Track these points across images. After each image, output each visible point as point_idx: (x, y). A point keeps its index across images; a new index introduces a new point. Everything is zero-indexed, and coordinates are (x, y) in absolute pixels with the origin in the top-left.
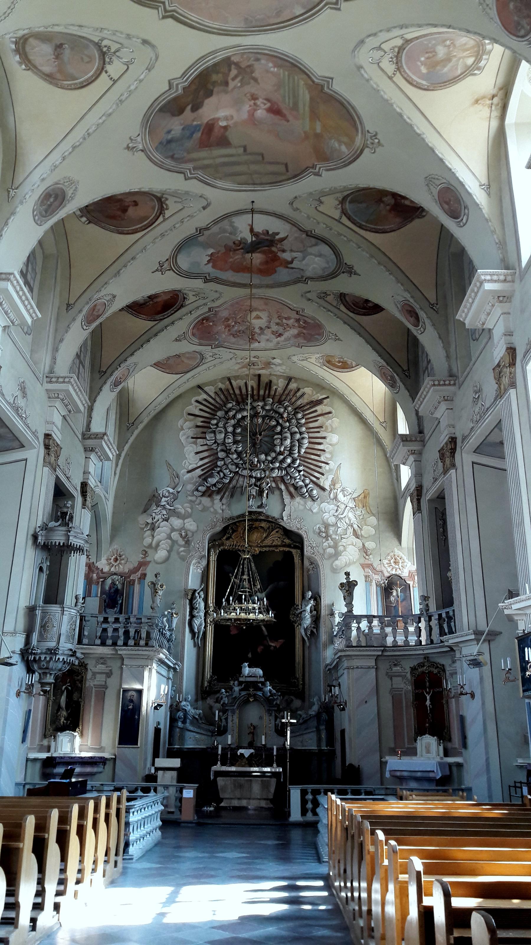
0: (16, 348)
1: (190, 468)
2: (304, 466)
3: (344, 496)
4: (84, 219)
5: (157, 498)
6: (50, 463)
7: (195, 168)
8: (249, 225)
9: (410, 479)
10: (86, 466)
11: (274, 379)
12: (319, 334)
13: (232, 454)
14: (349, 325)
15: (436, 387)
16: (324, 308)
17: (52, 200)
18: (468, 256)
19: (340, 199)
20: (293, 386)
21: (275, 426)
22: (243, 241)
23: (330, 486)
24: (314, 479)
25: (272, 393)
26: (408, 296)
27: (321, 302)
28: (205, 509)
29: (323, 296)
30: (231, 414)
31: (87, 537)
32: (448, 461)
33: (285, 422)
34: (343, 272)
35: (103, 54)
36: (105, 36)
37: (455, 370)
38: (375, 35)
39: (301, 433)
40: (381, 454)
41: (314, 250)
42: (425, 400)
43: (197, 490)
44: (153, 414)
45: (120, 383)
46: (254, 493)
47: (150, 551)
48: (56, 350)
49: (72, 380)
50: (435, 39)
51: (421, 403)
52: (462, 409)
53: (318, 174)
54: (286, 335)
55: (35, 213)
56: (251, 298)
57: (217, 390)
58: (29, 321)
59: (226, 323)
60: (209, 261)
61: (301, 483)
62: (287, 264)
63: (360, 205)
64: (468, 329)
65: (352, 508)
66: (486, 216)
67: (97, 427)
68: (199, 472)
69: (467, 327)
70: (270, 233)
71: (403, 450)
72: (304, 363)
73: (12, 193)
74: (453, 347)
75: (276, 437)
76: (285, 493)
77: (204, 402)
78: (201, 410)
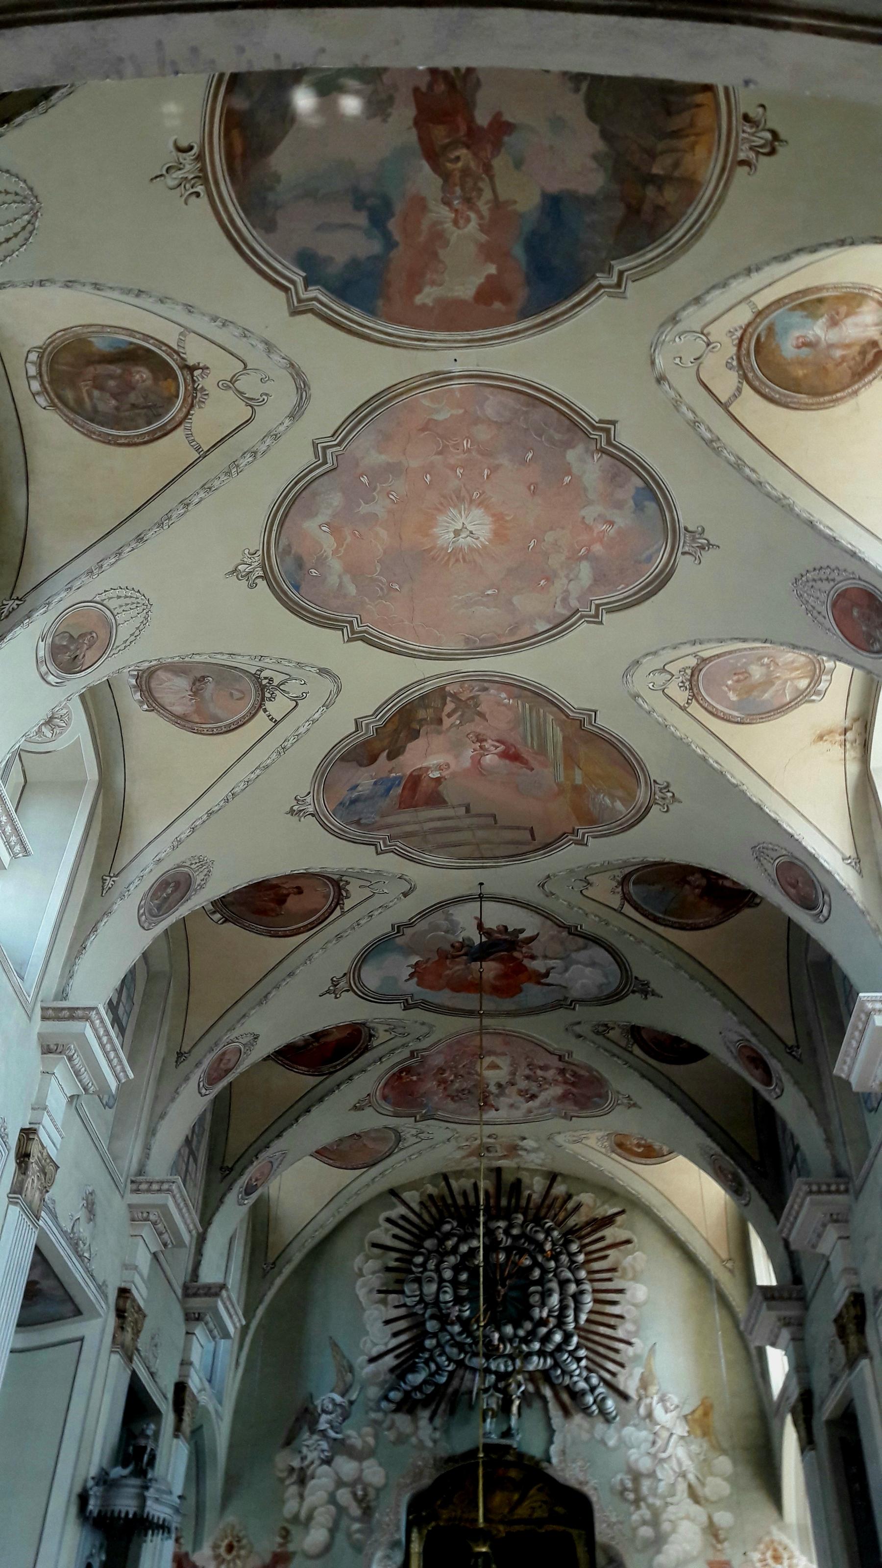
0: (86, 1133)
1: (375, 1352)
2: (588, 1349)
3: (666, 1412)
4: (217, 916)
5: (312, 1414)
6: (123, 1346)
7: (391, 838)
8: (476, 918)
9: (788, 1377)
10: (187, 1349)
11: (525, 1177)
12: (600, 1096)
13: (452, 1323)
14: (649, 1080)
15: (814, 1197)
16: (606, 1050)
17: (169, 891)
18: (839, 969)
19: (619, 879)
20: (560, 1189)
21: (530, 1269)
22: (467, 942)
23: (637, 1390)
24: (607, 1376)
25: (523, 1203)
26: (747, 1033)
27: (599, 1039)
28: (401, 1439)
29: (602, 1029)
30: (450, 1243)
31: (178, 1501)
32: (853, 1340)
33: (549, 1260)
34: (633, 992)
35: (263, 688)
36: (266, 666)
37: (844, 1165)
38: (655, 653)
39: (579, 1282)
40: (729, 1323)
41: (583, 955)
42: (799, 1221)
43: (386, 1398)
44: (310, 1244)
45: (255, 1188)
46: (494, 1406)
47: (294, 1530)
48: (152, 1132)
49: (174, 1187)
50: (744, 656)
51: (793, 1224)
52: (866, 1239)
53: (581, 843)
54: (543, 1096)
55: (142, 911)
56: (481, 1034)
57: (425, 1198)
58: (113, 1084)
59: (439, 1076)
60: (412, 976)
61: (582, 1385)
62: (539, 978)
63: (652, 888)
64: (858, 1094)
65: (682, 1438)
66: (860, 905)
67: (209, 1274)
68: (390, 1361)
69: (855, 1088)
70: (510, 929)
71: (768, 1317)
72: (577, 1148)
73: (109, 882)
74: (835, 1121)
75: (532, 1289)
76: (552, 1406)
77: (401, 1222)
78: (395, 1236)
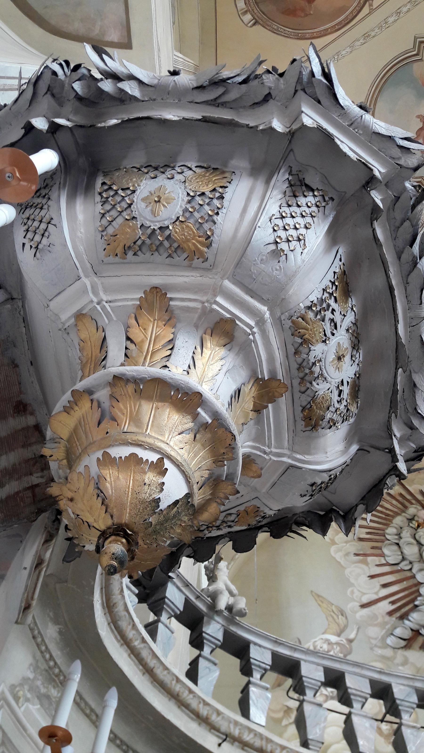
1: (365, 600)
4: (248, 17)
